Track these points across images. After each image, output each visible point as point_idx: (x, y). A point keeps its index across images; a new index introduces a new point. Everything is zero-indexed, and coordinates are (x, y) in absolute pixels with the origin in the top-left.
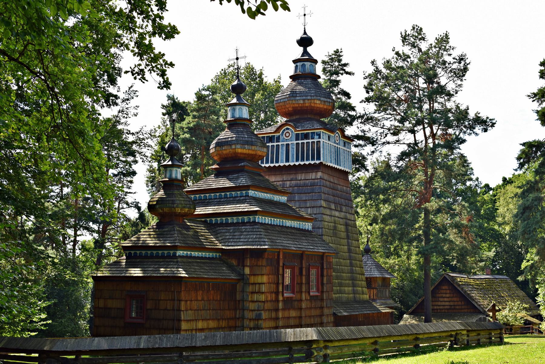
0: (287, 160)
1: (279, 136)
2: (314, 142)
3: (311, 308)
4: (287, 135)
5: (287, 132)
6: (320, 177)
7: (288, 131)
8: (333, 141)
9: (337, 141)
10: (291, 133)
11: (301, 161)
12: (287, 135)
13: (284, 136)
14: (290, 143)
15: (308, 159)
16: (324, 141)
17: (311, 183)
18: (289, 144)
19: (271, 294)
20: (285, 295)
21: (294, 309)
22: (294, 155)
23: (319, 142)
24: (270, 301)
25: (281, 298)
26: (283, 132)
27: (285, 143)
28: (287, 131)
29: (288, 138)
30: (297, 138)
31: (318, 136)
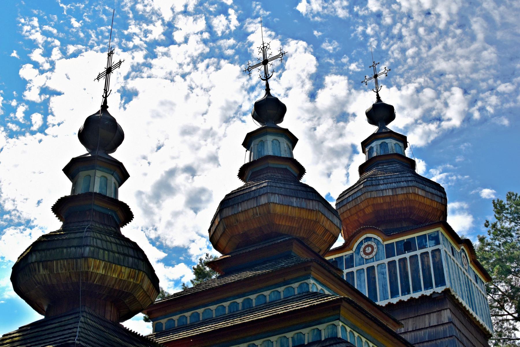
2: (427, 253)
5: (368, 246)
6: (449, 319)
7: (369, 243)
10: (375, 246)
11: (403, 294)
12: (368, 250)
13: (362, 253)
14: (375, 264)
15: (417, 289)
17: (429, 335)
18: (373, 267)
22: (386, 285)
23: (439, 250)
26: (359, 248)
28: (366, 244)
29: (371, 256)
30: (390, 251)
31: (433, 242)
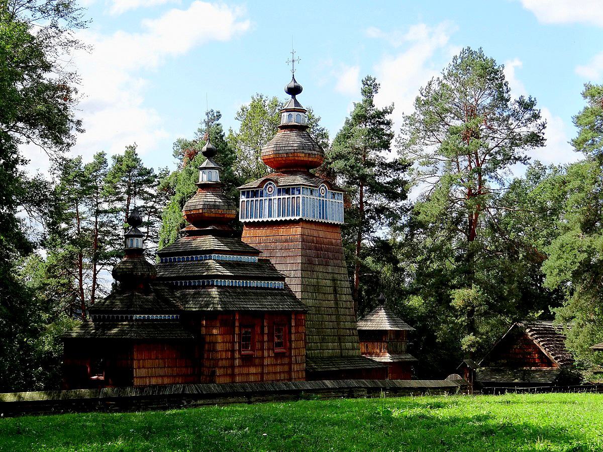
0: (270, 216)
1: (263, 191)
3: (276, 365)
4: (270, 189)
5: (270, 187)
7: (271, 186)
8: (318, 194)
9: (323, 194)
13: (267, 190)
16: (304, 196)
19: (226, 352)
20: (275, 350)
21: (255, 366)
24: (225, 359)
25: (237, 355)
26: (266, 187)
27: (268, 198)
28: (269, 186)
